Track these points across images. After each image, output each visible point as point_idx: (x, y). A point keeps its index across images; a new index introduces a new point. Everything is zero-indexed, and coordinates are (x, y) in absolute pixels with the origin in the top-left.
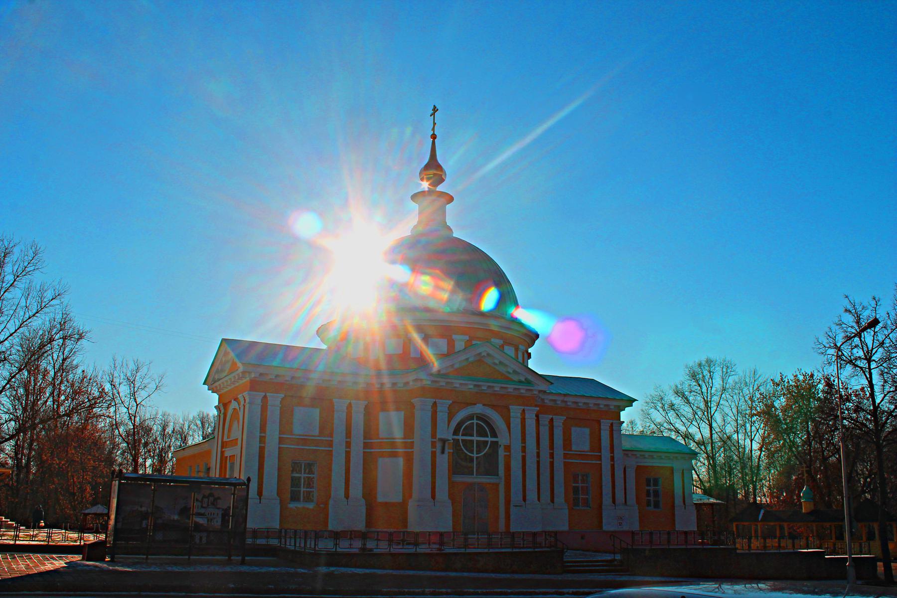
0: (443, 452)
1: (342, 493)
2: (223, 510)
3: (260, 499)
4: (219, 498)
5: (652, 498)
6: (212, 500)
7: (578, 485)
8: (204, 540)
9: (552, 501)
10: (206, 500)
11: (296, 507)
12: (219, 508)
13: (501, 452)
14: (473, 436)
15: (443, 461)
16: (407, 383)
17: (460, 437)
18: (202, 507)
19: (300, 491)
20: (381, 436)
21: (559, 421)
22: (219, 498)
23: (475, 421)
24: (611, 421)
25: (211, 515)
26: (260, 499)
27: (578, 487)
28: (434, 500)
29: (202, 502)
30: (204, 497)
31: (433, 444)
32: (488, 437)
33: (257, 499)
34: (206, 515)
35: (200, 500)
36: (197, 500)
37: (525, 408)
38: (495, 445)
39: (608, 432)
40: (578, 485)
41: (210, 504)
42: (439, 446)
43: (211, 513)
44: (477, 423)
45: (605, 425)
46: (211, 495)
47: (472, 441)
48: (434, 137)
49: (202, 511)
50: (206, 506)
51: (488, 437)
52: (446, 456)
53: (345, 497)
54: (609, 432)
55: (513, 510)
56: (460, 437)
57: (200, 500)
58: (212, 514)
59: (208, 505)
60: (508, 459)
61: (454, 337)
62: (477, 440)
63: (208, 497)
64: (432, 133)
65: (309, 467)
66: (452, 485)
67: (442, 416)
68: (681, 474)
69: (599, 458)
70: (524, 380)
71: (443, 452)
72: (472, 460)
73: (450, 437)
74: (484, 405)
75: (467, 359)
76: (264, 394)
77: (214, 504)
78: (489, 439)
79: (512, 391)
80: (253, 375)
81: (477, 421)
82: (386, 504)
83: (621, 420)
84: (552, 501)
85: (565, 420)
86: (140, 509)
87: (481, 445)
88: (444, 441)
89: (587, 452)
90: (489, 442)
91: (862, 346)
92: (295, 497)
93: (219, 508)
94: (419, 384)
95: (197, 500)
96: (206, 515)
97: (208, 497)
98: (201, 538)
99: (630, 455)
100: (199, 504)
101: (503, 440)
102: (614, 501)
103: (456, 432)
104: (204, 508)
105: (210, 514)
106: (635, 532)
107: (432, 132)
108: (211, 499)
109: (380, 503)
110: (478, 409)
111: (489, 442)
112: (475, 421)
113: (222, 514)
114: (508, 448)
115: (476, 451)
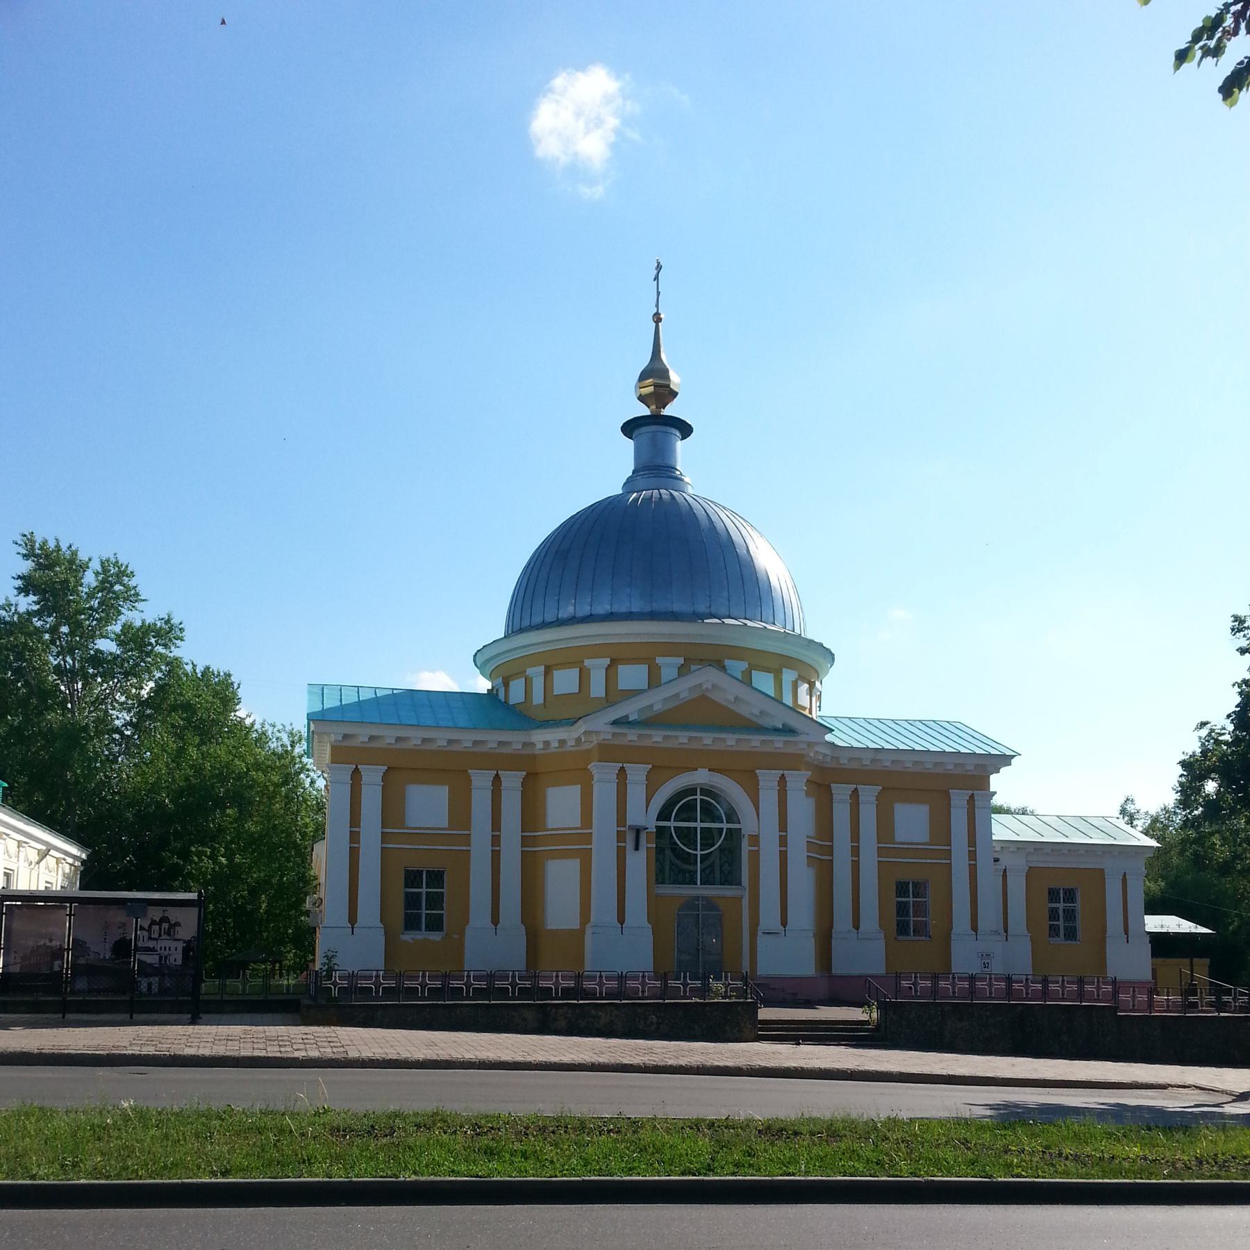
0: (637, 848)
2: (185, 941)
3: (353, 928)
4: (178, 924)
5: (1061, 923)
6: (167, 927)
8: (155, 988)
9: (856, 925)
10: (156, 928)
11: (413, 939)
12: (178, 940)
13: (745, 847)
15: (639, 864)
17: (672, 824)
18: (150, 938)
19: (420, 915)
20: (898, 839)
21: (869, 795)
22: (178, 924)
24: (972, 792)
25: (165, 949)
26: (353, 928)
27: (906, 904)
28: (785, 927)
29: (149, 930)
30: (153, 923)
31: (621, 837)
34: (157, 951)
35: (146, 927)
36: (142, 928)
37: (785, 772)
38: (735, 835)
39: (488, 795)
41: (163, 933)
42: (630, 838)
43: (165, 947)
45: (959, 799)
46: (165, 919)
48: (657, 318)
49: (151, 944)
50: (157, 936)
52: (642, 854)
54: (848, 806)
55: (762, 941)
57: (146, 927)
58: (167, 949)
59: (160, 935)
60: (755, 856)
61: (659, 660)
62: (701, 828)
63: (160, 923)
64: (655, 311)
65: (1070, 895)
66: (654, 902)
67: (636, 793)
69: (467, 839)
70: (781, 727)
71: (637, 848)
72: (689, 858)
73: (651, 823)
74: (709, 770)
75: (677, 695)
76: (354, 767)
77: (169, 934)
78: (725, 826)
79: (758, 745)
80: (333, 738)
82: (556, 933)
83: (991, 790)
84: (856, 925)
86: (48, 944)
88: (638, 831)
89: (446, 829)
90: (725, 831)
92: (412, 923)
93: (178, 940)
94: (595, 740)
95: (142, 928)
96: (157, 951)
97: (160, 923)
98: (150, 985)
100: (146, 934)
101: (748, 825)
102: (975, 928)
103: (664, 815)
104: (154, 939)
105: (163, 949)
106: (977, 976)
107: (656, 309)
108: (165, 925)
110: (701, 777)
111: (725, 831)
112: (698, 797)
113: (184, 948)
114: (755, 840)
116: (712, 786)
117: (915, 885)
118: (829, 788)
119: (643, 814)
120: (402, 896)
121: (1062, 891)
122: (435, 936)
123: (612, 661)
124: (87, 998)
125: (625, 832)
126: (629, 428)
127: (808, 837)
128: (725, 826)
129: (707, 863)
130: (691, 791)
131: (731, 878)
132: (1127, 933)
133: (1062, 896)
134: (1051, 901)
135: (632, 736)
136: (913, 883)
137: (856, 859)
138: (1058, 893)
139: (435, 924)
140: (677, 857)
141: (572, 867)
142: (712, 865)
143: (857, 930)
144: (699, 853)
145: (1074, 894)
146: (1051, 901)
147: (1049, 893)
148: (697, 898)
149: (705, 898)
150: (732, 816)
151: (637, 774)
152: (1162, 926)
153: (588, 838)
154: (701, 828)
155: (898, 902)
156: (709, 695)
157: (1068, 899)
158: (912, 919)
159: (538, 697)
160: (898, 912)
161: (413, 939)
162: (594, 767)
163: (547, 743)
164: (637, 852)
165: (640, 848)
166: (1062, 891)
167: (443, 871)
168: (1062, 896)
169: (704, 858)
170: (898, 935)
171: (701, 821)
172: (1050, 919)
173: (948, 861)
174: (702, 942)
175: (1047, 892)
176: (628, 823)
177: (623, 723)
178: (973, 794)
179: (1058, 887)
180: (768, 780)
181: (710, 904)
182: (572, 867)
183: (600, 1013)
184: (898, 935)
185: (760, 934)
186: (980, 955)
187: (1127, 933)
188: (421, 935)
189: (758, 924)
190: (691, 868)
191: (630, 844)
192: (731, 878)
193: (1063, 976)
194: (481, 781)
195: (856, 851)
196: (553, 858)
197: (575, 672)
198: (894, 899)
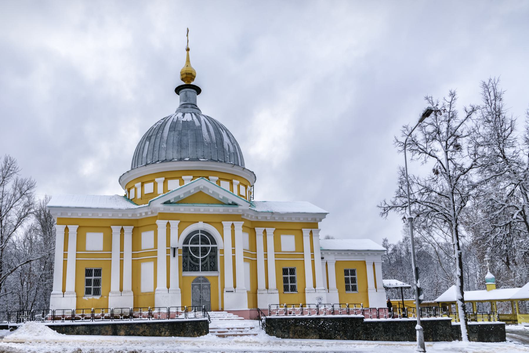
0: (174, 256)
1: (264, 287)
3: (64, 294)
7: (348, 277)
11: (88, 299)
13: (219, 255)
14: (199, 244)
15: (175, 263)
16: (146, 213)
17: (189, 246)
23: (200, 234)
26: (64, 294)
27: (287, 278)
28: (235, 288)
31: (168, 251)
32: (209, 244)
33: (178, 290)
37: (312, 229)
38: (214, 250)
40: (348, 277)
44: (201, 235)
47: (198, 248)
48: (188, 50)
51: (209, 244)
53: (266, 288)
55: (226, 295)
56: (189, 246)
62: (201, 247)
68: (325, 266)
69: (303, 256)
71: (174, 256)
72: (197, 261)
73: (180, 245)
74: (204, 222)
76: (66, 226)
78: (211, 246)
81: (201, 234)
85: (180, 223)
87: (205, 250)
91: (423, 151)
99: (370, 254)
101: (220, 245)
103: (186, 242)
109: (142, 293)
110: (201, 226)
112: (200, 234)
114: (222, 251)
115: (201, 254)
116: (205, 229)
117: (351, 271)
118: (254, 229)
119: (177, 242)
120: (357, 282)
121: (349, 271)
122: (97, 297)
123: (166, 179)
124: (418, 332)
125: (170, 249)
126: (178, 90)
127: (244, 250)
128: (211, 246)
129: (205, 262)
130: (197, 231)
131: (214, 268)
132: (376, 288)
133: (350, 273)
134: (345, 275)
135: (172, 209)
136: (290, 269)
137: (266, 259)
138: (348, 272)
139: (97, 292)
140: (192, 260)
141: (150, 265)
142: (207, 263)
143: (235, 288)
144: (200, 258)
145: (354, 271)
146: (345, 275)
147: (345, 272)
148: (200, 277)
149: (203, 277)
150: (214, 242)
151: (174, 224)
152: (390, 284)
153: (156, 253)
154: (201, 247)
155: (345, 278)
156: (202, 191)
157: (292, 273)
158: (351, 284)
159: (139, 196)
160: (345, 282)
161: (88, 299)
162: (158, 222)
163: (141, 214)
164: (175, 258)
165: (176, 256)
166: (349, 271)
167: (101, 269)
168: (350, 273)
169: (203, 260)
170: (284, 291)
171: (201, 244)
172: (284, 283)
173: (303, 259)
174: (202, 296)
175: (344, 271)
176: (171, 245)
177: (168, 203)
178: (311, 231)
179: (348, 269)
180: (227, 225)
181: (205, 279)
182: (150, 265)
183: (139, 328)
184: (284, 291)
185: (225, 291)
186: (317, 299)
187: (376, 288)
188: (90, 297)
189: (224, 287)
190: (197, 264)
191: (171, 255)
192: (214, 268)
193: (195, 307)
194: (116, 230)
195: (122, 255)
196: (144, 262)
197: (152, 184)
198: (282, 276)
